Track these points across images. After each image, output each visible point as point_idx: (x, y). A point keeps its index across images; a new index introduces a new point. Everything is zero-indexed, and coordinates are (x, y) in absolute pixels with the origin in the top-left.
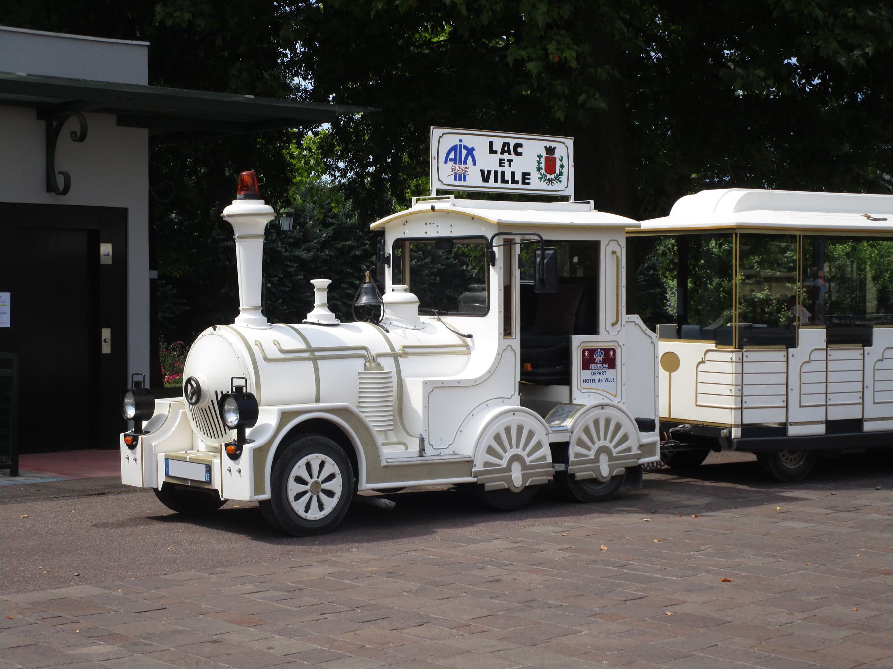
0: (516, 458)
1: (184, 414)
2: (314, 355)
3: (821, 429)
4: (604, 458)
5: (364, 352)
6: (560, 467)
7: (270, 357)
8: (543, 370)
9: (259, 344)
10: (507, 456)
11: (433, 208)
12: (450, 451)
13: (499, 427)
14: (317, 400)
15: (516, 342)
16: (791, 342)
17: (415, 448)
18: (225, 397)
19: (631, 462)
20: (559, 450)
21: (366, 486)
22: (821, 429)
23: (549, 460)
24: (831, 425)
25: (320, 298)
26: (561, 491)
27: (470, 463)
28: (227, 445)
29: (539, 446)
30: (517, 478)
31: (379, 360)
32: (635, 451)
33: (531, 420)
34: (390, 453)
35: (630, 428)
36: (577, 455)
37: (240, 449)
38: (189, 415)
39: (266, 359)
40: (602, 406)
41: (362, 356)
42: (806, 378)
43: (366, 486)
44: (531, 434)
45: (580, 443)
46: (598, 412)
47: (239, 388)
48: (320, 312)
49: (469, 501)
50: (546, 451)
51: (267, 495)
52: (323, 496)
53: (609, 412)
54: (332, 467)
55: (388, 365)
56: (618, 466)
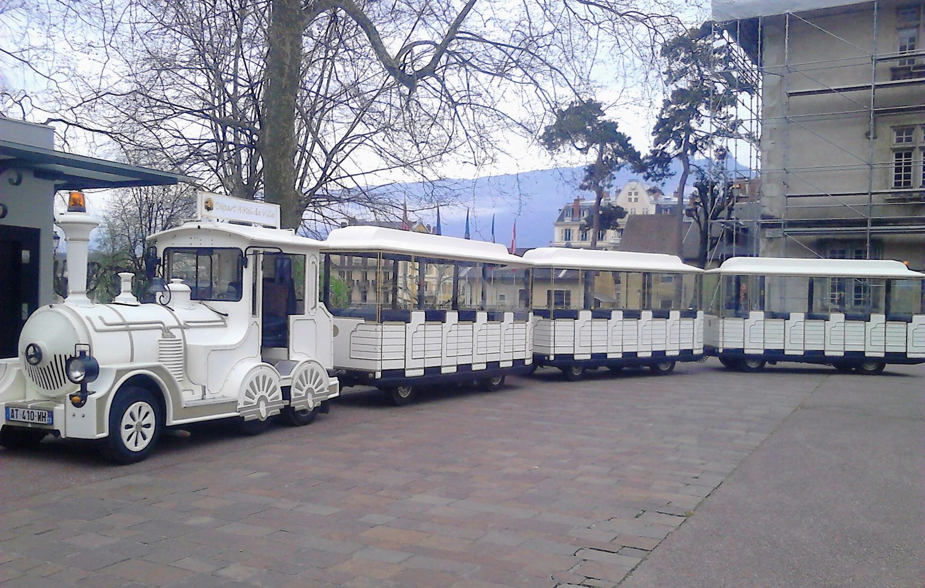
0: (262, 398)
1: (20, 372)
2: (127, 327)
3: (589, 357)
4: (262, 404)
5: (161, 325)
6: (287, 402)
7: (98, 328)
8: (275, 336)
9: (89, 319)
10: (257, 397)
11: (199, 227)
12: (220, 395)
13: (252, 378)
14: (132, 360)
15: (259, 320)
16: (407, 320)
17: (198, 394)
18: (69, 361)
19: (324, 398)
20: (286, 391)
21: (171, 421)
22: (589, 357)
23: (281, 398)
24: (593, 355)
25: (126, 286)
26: (288, 418)
27: (235, 403)
28: (71, 396)
29: (274, 389)
30: (264, 412)
31: (171, 331)
32: (326, 391)
33: (269, 372)
34: (190, 397)
35: (324, 375)
36: (296, 394)
37: (84, 399)
38: (26, 373)
39: (96, 331)
40: (308, 362)
41: (161, 328)
42: (583, 333)
43: (171, 421)
44: (270, 381)
45: (298, 387)
46: (307, 365)
47: (83, 353)
48: (126, 296)
49: (230, 429)
50: (279, 392)
51: (105, 434)
52: (144, 429)
53: (312, 365)
54: (146, 407)
55: (177, 333)
56: (317, 400)
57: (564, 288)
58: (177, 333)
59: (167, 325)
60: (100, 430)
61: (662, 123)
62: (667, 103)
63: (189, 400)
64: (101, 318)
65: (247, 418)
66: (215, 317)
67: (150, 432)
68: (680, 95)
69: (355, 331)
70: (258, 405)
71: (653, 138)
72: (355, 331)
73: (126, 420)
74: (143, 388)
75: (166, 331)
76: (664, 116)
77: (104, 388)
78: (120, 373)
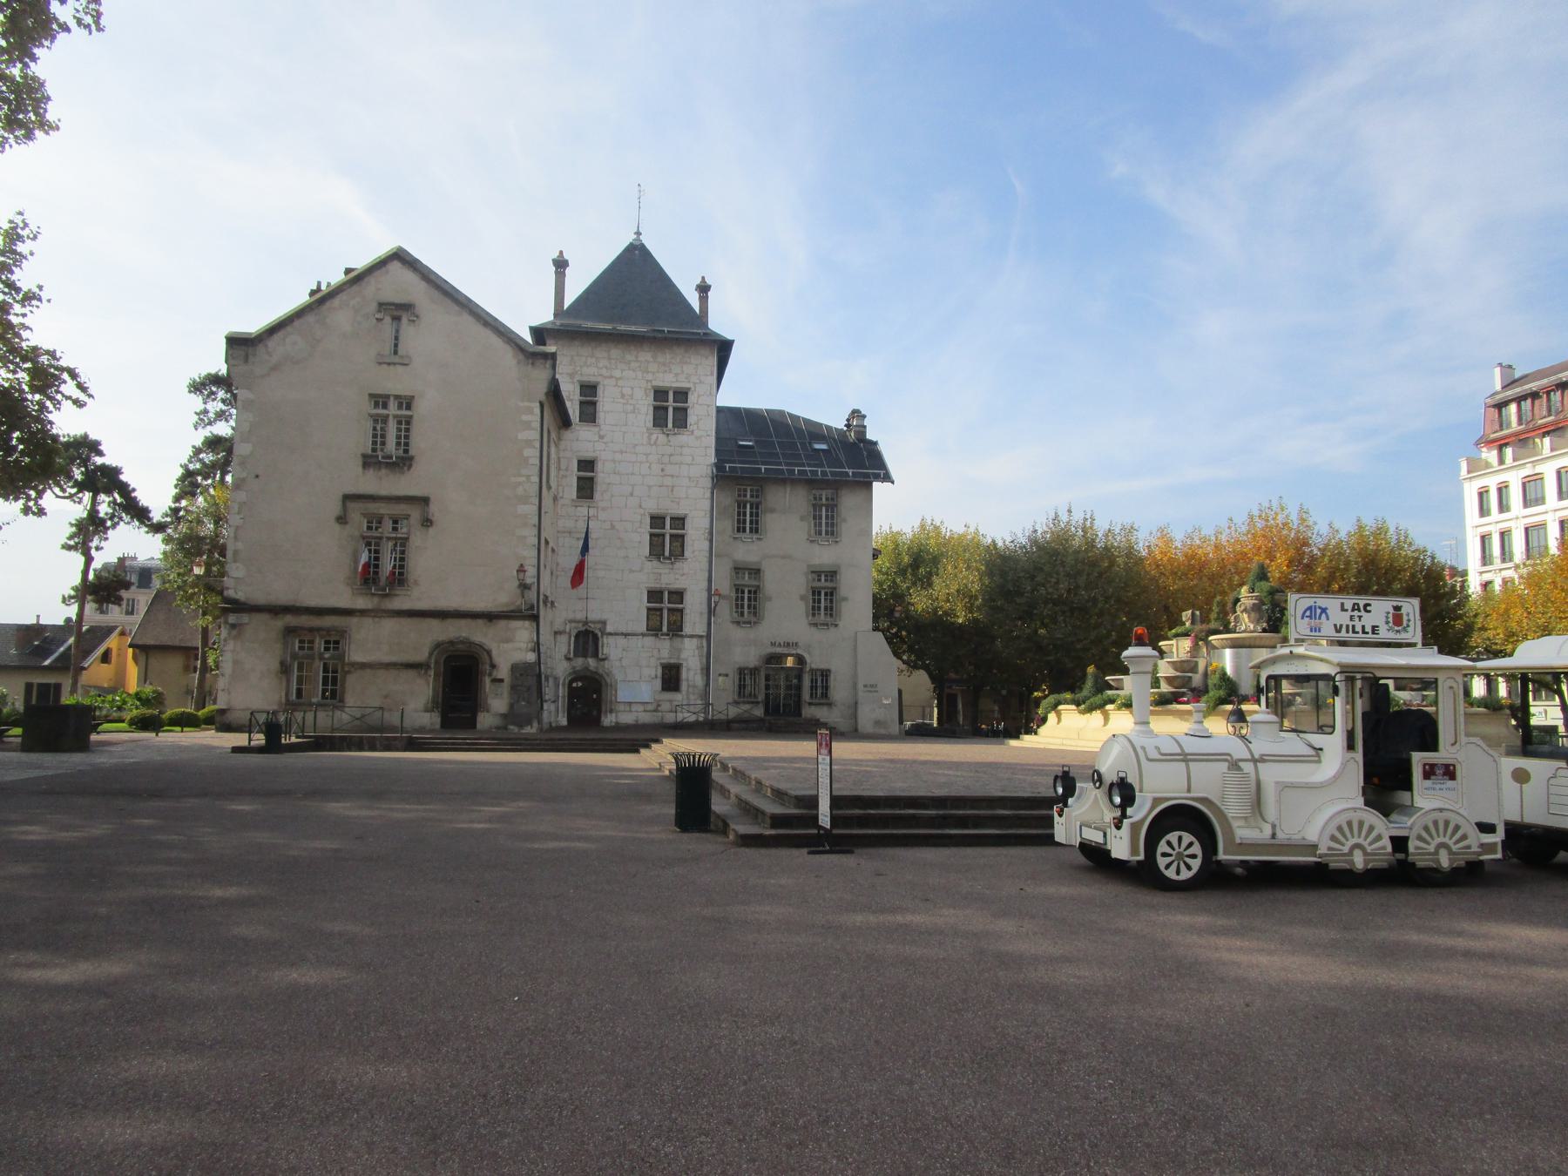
0: (1357, 846)
6: (1400, 856)
9: (1143, 748)
14: (1189, 790)
15: (1359, 755)
17: (1268, 831)
21: (1222, 856)
27: (1315, 847)
30: (1359, 862)
45: (1420, 838)
51: (1141, 857)
54: (1188, 838)
55: (1248, 767)
57: (50, 679)
58: (1248, 767)
59: (1236, 757)
60: (1134, 851)
61: (188, 475)
62: (197, 451)
63: (1244, 834)
64: (1157, 748)
65: (1333, 865)
66: (1312, 752)
67: (1196, 864)
68: (214, 443)
69: (1554, 776)
70: (1436, 853)
71: (174, 491)
72: (1554, 776)
73: (1162, 847)
74: (1183, 817)
75: (1235, 765)
76: (191, 467)
77: (1141, 811)
78: (1157, 801)
